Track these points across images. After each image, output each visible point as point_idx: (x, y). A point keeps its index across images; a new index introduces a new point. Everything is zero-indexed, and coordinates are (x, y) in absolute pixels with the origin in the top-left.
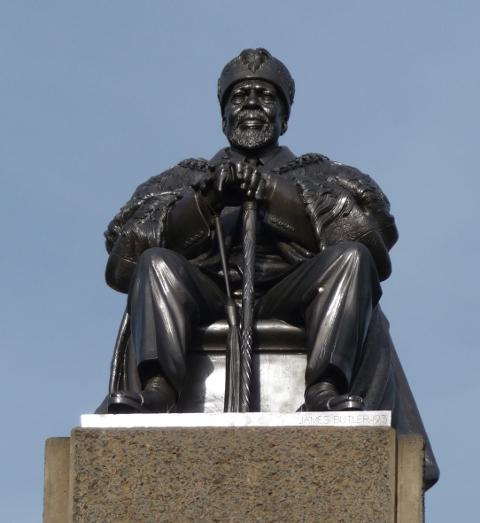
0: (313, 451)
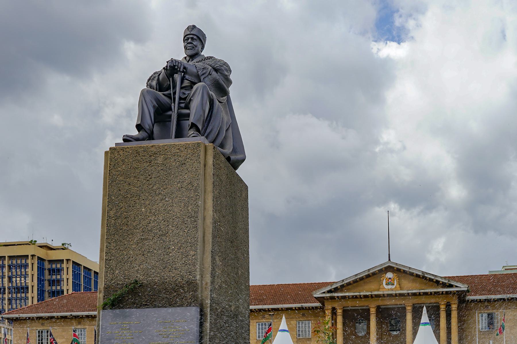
0: (178, 151)
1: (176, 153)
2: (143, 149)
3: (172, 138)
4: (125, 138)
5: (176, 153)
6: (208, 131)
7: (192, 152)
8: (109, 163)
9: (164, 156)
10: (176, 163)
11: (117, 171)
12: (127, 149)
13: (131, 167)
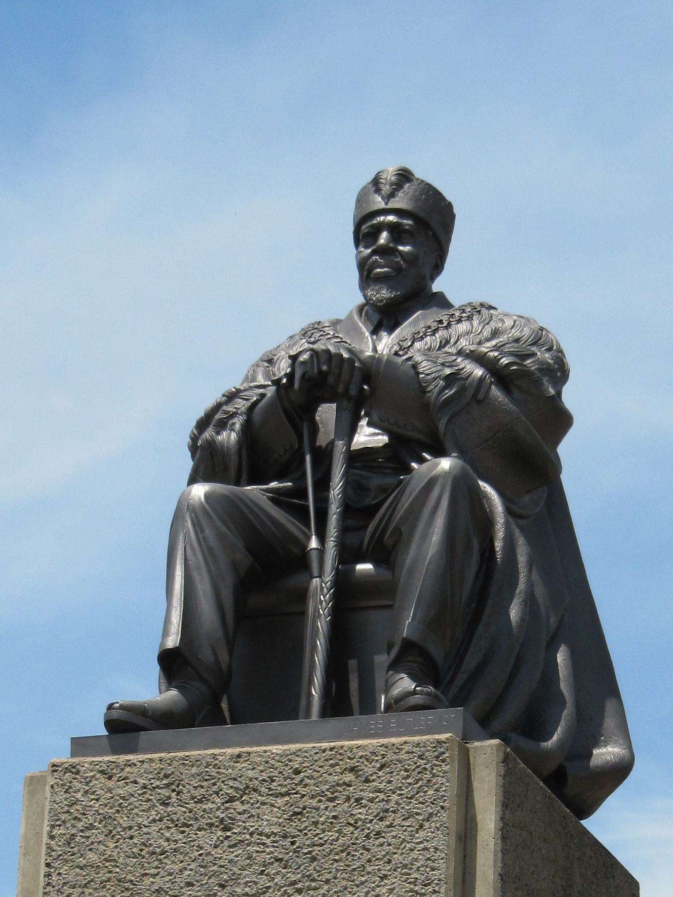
0: (349, 777)
1: (338, 785)
2: (194, 770)
3: (308, 715)
4: (115, 714)
5: (338, 785)
6: (471, 661)
7: (410, 781)
8: (46, 829)
9: (287, 798)
10: (339, 832)
11: (81, 868)
12: (128, 769)
13: (141, 850)
